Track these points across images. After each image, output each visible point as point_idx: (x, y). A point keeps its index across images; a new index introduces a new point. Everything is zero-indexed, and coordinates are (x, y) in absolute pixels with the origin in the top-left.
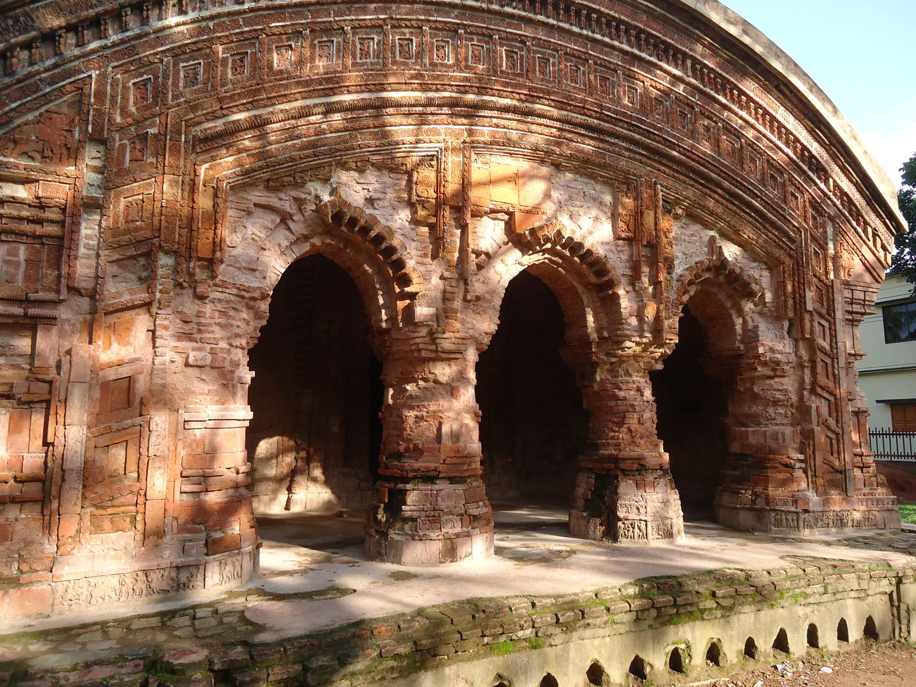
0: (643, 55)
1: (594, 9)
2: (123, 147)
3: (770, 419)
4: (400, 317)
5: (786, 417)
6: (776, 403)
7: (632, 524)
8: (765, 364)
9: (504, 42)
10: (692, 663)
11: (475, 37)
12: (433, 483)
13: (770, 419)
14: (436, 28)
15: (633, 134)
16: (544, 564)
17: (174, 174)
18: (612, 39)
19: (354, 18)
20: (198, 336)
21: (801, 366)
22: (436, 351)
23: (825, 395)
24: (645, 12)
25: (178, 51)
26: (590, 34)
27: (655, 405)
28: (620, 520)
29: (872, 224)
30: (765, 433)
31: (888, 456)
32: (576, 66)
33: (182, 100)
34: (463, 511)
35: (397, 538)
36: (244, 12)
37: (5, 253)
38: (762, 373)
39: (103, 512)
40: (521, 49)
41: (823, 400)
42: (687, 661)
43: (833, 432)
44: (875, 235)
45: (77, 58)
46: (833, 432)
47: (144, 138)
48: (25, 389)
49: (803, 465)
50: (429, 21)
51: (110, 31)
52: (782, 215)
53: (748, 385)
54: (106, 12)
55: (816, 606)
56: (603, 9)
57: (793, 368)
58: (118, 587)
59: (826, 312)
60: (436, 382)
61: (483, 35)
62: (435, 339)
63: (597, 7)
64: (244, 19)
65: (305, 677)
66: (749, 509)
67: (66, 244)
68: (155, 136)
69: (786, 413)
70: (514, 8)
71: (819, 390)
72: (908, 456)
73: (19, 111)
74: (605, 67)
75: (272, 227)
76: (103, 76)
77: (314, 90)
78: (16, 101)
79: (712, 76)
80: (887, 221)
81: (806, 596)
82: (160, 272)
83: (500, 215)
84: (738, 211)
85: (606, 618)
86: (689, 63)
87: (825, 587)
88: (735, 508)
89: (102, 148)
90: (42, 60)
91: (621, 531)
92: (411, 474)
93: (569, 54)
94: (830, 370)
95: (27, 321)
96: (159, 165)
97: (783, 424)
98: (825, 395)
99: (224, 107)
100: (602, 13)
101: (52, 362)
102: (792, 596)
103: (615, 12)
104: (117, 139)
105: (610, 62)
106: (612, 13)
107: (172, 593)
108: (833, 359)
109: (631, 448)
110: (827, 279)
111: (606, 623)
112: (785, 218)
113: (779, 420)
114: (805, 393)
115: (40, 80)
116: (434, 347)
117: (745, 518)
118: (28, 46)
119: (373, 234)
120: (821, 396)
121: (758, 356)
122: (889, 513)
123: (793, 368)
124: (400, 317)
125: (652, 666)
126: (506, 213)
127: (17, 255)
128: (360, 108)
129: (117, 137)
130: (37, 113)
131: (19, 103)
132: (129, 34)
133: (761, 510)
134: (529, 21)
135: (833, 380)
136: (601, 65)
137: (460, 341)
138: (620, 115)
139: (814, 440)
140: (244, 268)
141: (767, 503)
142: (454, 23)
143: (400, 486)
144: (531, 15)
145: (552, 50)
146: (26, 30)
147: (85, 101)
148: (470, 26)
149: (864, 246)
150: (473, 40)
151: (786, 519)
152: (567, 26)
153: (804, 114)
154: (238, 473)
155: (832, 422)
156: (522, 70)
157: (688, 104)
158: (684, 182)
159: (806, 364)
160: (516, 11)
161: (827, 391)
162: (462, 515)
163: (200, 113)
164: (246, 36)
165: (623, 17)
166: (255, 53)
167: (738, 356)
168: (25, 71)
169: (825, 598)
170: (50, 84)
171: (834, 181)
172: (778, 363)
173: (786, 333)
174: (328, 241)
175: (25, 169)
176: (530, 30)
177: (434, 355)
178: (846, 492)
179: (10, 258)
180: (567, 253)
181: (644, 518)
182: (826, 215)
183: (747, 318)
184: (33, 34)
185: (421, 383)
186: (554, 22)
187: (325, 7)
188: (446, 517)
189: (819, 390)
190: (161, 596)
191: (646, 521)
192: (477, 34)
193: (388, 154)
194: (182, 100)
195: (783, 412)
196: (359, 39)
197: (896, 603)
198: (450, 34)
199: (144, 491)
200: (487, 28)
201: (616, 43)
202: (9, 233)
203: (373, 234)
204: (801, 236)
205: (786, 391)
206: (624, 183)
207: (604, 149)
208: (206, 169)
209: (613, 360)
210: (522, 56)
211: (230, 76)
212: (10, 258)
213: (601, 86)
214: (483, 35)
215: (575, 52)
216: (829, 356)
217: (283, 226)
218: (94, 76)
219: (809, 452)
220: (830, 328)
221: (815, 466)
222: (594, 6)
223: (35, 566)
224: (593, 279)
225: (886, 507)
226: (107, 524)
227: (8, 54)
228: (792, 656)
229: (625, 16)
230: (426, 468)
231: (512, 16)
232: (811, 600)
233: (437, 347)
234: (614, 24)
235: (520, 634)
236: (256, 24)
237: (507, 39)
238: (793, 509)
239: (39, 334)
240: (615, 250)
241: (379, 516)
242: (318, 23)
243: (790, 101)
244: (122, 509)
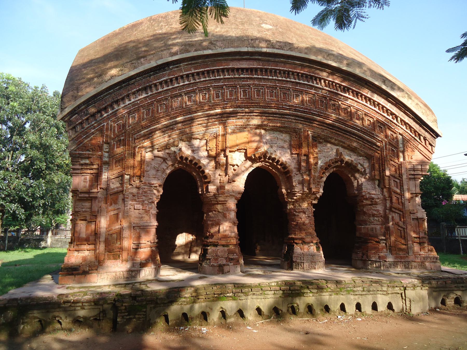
0: (301, 82)
1: (277, 69)
2: (114, 144)
3: (371, 223)
4: (205, 190)
5: (379, 221)
6: (374, 215)
8: (367, 199)
9: (242, 87)
10: (299, 311)
12: (217, 247)
13: (371, 223)
14: (215, 88)
15: (297, 113)
19: (185, 90)
20: (138, 200)
21: (385, 199)
22: (217, 201)
23: (397, 211)
24: (300, 66)
26: (277, 78)
27: (313, 217)
29: (423, 135)
30: (368, 228)
32: (272, 91)
33: (131, 127)
34: (227, 257)
35: (205, 265)
36: (149, 96)
38: (366, 203)
39: (111, 254)
40: (249, 89)
41: (396, 214)
42: (297, 310)
43: (402, 227)
44: (425, 139)
45: (101, 120)
46: (402, 227)
47: (120, 140)
48: (89, 218)
49: (385, 242)
51: (110, 110)
52: (373, 136)
53: (362, 208)
54: (108, 105)
55: (360, 296)
56: (281, 68)
57: (382, 200)
58: (115, 276)
59: (398, 175)
60: (218, 212)
63: (278, 68)
64: (149, 98)
65: (157, 301)
66: (360, 260)
68: (123, 139)
69: (379, 220)
70: (244, 75)
71: (393, 210)
72: (464, 237)
74: (285, 89)
75: (160, 163)
76: (108, 124)
79: (334, 84)
80: (431, 133)
81: (354, 291)
82: (125, 181)
83: (241, 151)
84: (349, 137)
85: (261, 292)
86: (322, 81)
87: (363, 288)
88: (356, 260)
89: (108, 145)
90: (91, 122)
92: (209, 244)
93: (269, 87)
94: (400, 200)
95: (90, 198)
97: (377, 225)
98: (397, 211)
101: (96, 210)
102: (347, 291)
103: (286, 68)
104: (112, 142)
105: (286, 87)
106: (285, 69)
107: (130, 279)
108: (401, 196)
109: (300, 234)
110: (398, 161)
111: (261, 294)
112: (374, 137)
113: (375, 222)
114: (387, 211)
116: (216, 200)
117: (359, 264)
118: (87, 119)
119: (193, 162)
120: (395, 212)
121: (363, 196)
122: (433, 263)
123: (382, 200)
124: (205, 190)
125: (282, 311)
126: (244, 149)
128: (187, 121)
129: (112, 141)
132: (114, 110)
133: (365, 260)
135: (401, 205)
136: (282, 88)
137: (225, 197)
138: (291, 107)
139: (389, 231)
141: (367, 257)
144: (251, 76)
145: (262, 87)
146: (87, 115)
148: (227, 84)
149: (420, 145)
150: (229, 89)
152: (266, 77)
153: (381, 93)
154: (151, 243)
155: (401, 224)
156: (249, 96)
157: (323, 97)
159: (387, 199)
160: (245, 76)
161: (398, 210)
162: (227, 258)
164: (149, 103)
165: (290, 70)
166: (153, 108)
167: (356, 196)
168: (87, 126)
169: (364, 293)
170: (94, 129)
171: (401, 119)
172: (373, 199)
173: (377, 186)
174: (180, 165)
176: (252, 81)
177: (217, 203)
178: (408, 253)
180: (271, 161)
181: (302, 261)
182: (398, 133)
183: (359, 180)
184: (89, 115)
185: (214, 212)
186: (261, 77)
188: (220, 259)
189: (393, 210)
190: (127, 279)
192: (231, 87)
195: (377, 219)
197: (404, 298)
198: (221, 89)
201: (288, 79)
203: (193, 162)
204: (383, 144)
205: (378, 210)
206: (294, 132)
207: (284, 121)
209: (293, 200)
210: (249, 91)
211: (145, 117)
213: (283, 96)
215: (271, 86)
216: (399, 195)
217: (164, 162)
219: (388, 236)
221: (390, 242)
222: (277, 68)
223: (93, 269)
225: (432, 260)
226: (112, 257)
228: (347, 314)
229: (291, 69)
230: (214, 241)
231: (244, 78)
232: (357, 293)
234: (287, 72)
235: (228, 295)
237: (242, 86)
239: (93, 201)
240: (291, 159)
243: (373, 88)
244: (116, 253)
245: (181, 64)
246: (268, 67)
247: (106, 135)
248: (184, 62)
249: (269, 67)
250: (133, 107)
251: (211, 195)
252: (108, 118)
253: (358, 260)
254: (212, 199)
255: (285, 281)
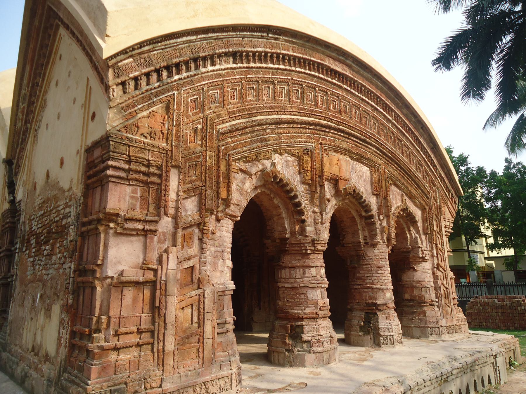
1: (364, 85)
7: (386, 338)
11: (321, 92)
16: (249, 363)
17: (211, 151)
18: (368, 99)
23: (442, 270)
25: (210, 85)
28: (381, 336)
31: (465, 298)
32: (355, 110)
37: (131, 192)
50: (305, 82)
61: (324, 91)
62: (315, 244)
67: (163, 188)
71: (440, 269)
73: (141, 110)
74: (365, 112)
77: (265, 112)
78: (140, 104)
88: (411, 327)
91: (382, 342)
96: (203, 146)
98: (442, 270)
99: (231, 116)
100: (366, 87)
105: (367, 110)
106: (369, 88)
115: (151, 93)
116: (313, 248)
127: (137, 193)
130: (148, 112)
131: (142, 105)
134: (341, 87)
140: (236, 204)
142: (314, 85)
143: (299, 323)
144: (342, 85)
147: (171, 107)
148: (320, 86)
149: (448, 202)
151: (435, 331)
158: (394, 169)
163: (221, 119)
164: (237, 80)
165: (373, 90)
170: (156, 97)
175: (144, 144)
179: (133, 195)
181: (392, 334)
187: (268, 70)
189: (440, 269)
191: (393, 336)
193: (292, 147)
194: (211, 111)
196: (280, 87)
198: (312, 89)
199: (202, 333)
200: (326, 89)
202: (134, 180)
208: (223, 149)
212: (133, 195)
214: (324, 91)
218: (175, 94)
220: (441, 239)
224: (364, 214)
227: (139, 78)
233: (315, 248)
236: (242, 75)
238: (437, 326)
241: (287, 341)
242: (265, 77)
245: (281, 37)
246: (357, 80)
247: (176, 112)
248: (286, 36)
249: (359, 81)
250: (216, 78)
251: (308, 241)
252: (179, 86)
253: (415, 327)
254: (308, 247)
255: (292, 364)
